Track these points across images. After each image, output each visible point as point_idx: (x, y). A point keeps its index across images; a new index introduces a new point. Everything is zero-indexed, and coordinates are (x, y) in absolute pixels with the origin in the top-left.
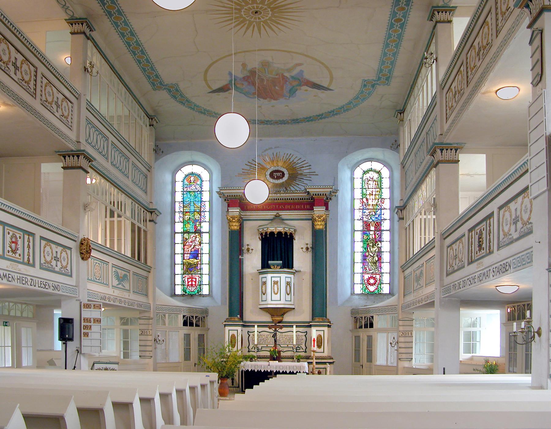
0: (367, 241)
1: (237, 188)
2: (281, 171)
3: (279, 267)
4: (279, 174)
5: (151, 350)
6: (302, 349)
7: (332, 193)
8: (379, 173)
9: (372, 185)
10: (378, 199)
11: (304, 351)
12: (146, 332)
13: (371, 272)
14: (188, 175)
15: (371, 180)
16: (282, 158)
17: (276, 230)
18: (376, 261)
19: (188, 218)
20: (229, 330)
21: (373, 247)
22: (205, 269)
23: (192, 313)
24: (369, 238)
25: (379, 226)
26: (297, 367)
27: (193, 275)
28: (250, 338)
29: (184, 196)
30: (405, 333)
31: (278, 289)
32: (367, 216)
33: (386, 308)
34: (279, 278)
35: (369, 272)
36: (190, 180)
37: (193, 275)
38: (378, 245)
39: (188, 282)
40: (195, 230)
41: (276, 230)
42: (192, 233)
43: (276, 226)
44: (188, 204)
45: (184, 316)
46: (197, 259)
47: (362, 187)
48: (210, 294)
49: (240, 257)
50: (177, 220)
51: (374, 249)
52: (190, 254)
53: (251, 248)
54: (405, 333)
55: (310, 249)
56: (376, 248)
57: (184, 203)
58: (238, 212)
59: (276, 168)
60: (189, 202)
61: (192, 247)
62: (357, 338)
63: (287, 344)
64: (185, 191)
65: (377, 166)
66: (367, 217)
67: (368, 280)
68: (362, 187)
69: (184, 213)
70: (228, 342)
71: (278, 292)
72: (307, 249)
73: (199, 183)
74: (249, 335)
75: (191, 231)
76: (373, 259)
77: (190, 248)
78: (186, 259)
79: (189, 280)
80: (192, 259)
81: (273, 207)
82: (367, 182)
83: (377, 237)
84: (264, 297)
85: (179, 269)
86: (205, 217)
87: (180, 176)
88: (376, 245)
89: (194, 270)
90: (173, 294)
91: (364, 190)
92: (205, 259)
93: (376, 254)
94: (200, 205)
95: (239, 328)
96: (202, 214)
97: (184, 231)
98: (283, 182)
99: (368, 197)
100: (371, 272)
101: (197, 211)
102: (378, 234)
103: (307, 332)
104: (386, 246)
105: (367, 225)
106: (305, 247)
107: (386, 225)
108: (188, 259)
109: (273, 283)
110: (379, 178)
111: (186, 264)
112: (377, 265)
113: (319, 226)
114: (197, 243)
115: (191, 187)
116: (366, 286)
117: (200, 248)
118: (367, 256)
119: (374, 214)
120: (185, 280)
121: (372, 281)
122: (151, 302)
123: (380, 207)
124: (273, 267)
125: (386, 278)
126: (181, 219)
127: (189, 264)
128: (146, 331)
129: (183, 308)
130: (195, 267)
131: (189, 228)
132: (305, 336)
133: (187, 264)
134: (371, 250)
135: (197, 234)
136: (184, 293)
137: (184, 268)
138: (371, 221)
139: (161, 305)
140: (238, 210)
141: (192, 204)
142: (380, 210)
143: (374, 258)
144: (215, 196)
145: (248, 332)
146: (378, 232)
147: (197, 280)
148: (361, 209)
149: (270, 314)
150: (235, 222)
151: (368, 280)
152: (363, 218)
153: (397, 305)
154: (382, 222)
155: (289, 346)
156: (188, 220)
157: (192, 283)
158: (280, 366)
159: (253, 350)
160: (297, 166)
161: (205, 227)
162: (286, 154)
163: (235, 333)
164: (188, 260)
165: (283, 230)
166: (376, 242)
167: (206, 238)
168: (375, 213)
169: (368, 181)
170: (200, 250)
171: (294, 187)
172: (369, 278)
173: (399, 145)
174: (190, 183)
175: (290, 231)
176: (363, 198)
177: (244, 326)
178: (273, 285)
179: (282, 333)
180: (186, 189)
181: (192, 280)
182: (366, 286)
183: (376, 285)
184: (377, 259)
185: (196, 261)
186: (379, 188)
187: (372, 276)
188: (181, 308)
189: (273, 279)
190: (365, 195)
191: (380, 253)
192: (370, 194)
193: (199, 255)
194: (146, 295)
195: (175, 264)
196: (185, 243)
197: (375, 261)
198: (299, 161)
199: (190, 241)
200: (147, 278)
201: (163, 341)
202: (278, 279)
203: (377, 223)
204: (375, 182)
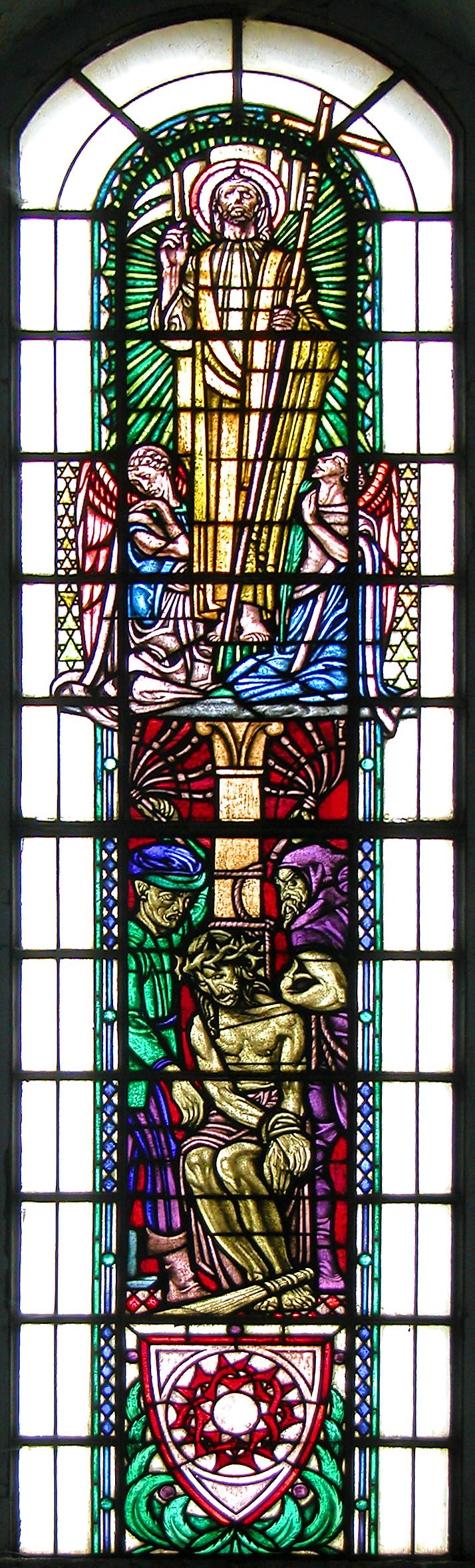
0: (172, 951)
10: (312, 460)
13: (224, 1303)
18: (297, 1181)
24: (197, 915)
25: (314, 759)
27: (310, 418)
32: (173, 657)
35: (199, 1307)
37: (310, 418)
38: (300, 986)
47: (120, 313)
51: (263, 1033)
56: (281, 1021)
66: (177, 671)
68: (120, 313)
76: (258, 1160)
88: (286, 982)
93: (291, 1103)
100: (224, 1303)
102: (300, 872)
112: (305, 1224)
116: (173, 1469)
118: (193, 1129)
119: (251, 627)
123: (339, 551)
134: (228, 1038)
142: (335, 592)
143: (273, 1153)
148: (103, 578)
152: (125, 679)
168: (270, 625)
182: (173, 1469)
183: (281, 1451)
186: (332, 334)
187: (232, 1358)
190: (151, 410)
197: (279, 1182)
203: (293, 725)
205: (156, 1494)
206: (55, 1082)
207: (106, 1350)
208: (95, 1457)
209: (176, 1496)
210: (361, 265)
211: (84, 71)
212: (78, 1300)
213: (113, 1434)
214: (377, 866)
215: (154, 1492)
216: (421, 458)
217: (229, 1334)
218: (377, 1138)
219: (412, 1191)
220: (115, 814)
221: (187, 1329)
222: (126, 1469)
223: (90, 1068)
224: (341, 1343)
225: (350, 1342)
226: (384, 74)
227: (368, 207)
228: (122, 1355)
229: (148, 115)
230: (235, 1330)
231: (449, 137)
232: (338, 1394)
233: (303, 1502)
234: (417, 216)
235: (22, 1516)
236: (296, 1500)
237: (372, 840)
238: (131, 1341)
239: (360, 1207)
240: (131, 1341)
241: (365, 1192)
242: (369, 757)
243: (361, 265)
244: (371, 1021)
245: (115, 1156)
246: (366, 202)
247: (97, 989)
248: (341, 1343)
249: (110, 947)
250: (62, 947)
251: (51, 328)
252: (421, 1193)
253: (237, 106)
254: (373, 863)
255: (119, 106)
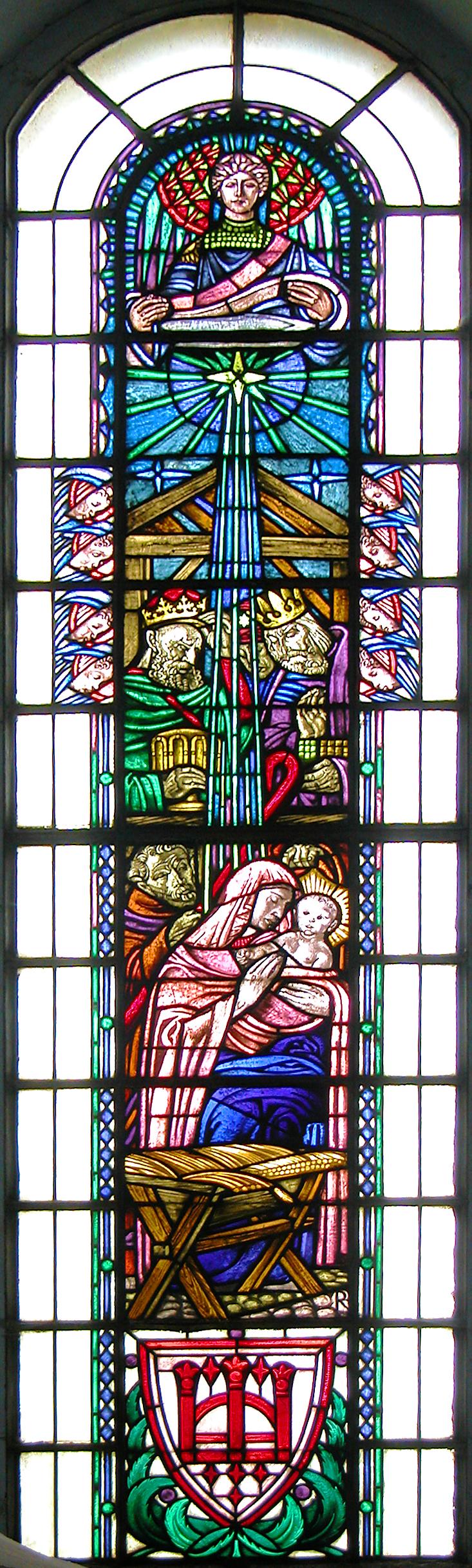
205: (157, 1498)
206: (53, 1454)
207: (105, 1431)
208: (96, 1294)
209: (176, 1499)
210: (365, 259)
211: (81, 68)
212: (77, 1307)
213: (113, 1439)
214: (377, 870)
215: (154, 1495)
216: (422, 459)
217: (230, 1338)
218: (378, 860)
219: (415, 1195)
220: (114, 1552)
221: (187, 1335)
222: (127, 1473)
223: (88, 1318)
224: (342, 1345)
225: (353, 1344)
226: (392, 66)
227: (372, 202)
228: (122, 1361)
229: (146, 113)
230: (235, 1333)
231: (456, 130)
232: (340, 1396)
233: (307, 1502)
234: (424, 210)
235: (20, 1277)
236: (297, 1500)
237: (372, 844)
238: (130, 1346)
239: (361, 1452)
240: (130, 1346)
241: (367, 1195)
242: (370, 762)
243: (365, 259)
244: (372, 773)
245: (112, 1183)
246: (371, 197)
247: (93, 746)
248: (342, 1345)
249: (106, 954)
250: (58, 955)
251: (49, 456)
252: (423, 952)
253: (238, 103)
254: (374, 866)
255: (118, 103)
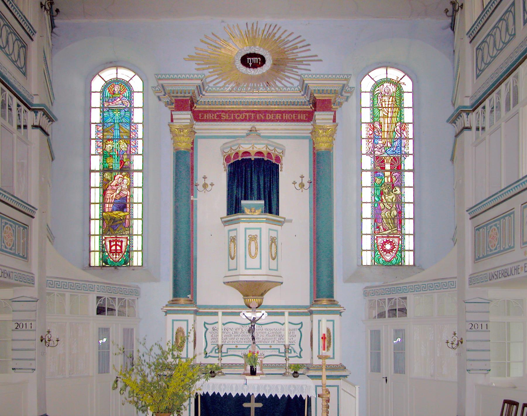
1: (187, 76)
2: (260, 55)
3: (258, 212)
4: (255, 60)
5: (33, 358)
6: (295, 352)
7: (343, 93)
8: (397, 84)
9: (387, 103)
11: (297, 356)
12: (24, 326)
14: (110, 83)
15: (386, 94)
16: (261, 33)
17: (253, 148)
19: (111, 148)
20: (173, 321)
21: (389, 194)
22: (137, 227)
23: (113, 294)
24: (383, 182)
26: (295, 388)
28: (209, 335)
29: (105, 114)
30: (476, 325)
31: (256, 248)
32: (380, 149)
33: (433, 282)
34: (259, 230)
35: (384, 233)
36: (114, 90)
38: (395, 191)
39: (111, 247)
40: (121, 168)
41: (253, 148)
42: (117, 171)
43: (254, 142)
44: (110, 128)
45: (98, 298)
46: (123, 212)
47: (373, 105)
48: (145, 265)
49: (192, 198)
50: (93, 151)
51: (391, 197)
52: (113, 203)
53: (208, 182)
54: (476, 325)
55: (307, 185)
56: (393, 195)
57: (103, 126)
58: (187, 119)
59: (252, 51)
60: (112, 124)
61: (118, 192)
62: (376, 335)
63: (270, 343)
64: (106, 108)
65: (394, 74)
67: (383, 245)
69: (105, 141)
70: (171, 342)
71: (256, 254)
72: (302, 185)
73: (126, 94)
74: (207, 329)
75: (116, 169)
77: (115, 194)
78: (107, 210)
79: (112, 244)
80: (117, 212)
81: (246, 116)
82: (380, 97)
83: (394, 181)
84: (233, 263)
85: (95, 227)
86: (136, 147)
87: (97, 84)
88: (393, 191)
89: (119, 228)
90: (88, 265)
91: (376, 111)
92: (137, 211)
94: (128, 128)
95: (190, 317)
96: (132, 143)
97: (103, 168)
98: (263, 73)
99: (382, 120)
100: (386, 232)
101: (125, 137)
102: (395, 176)
103: (302, 323)
104: (408, 195)
105: (379, 161)
106: (299, 181)
107: (408, 163)
108: (111, 212)
109: (248, 238)
110: (398, 92)
111: (107, 219)
112: (396, 222)
113: (323, 146)
114: (124, 187)
115: (115, 101)
116: (381, 254)
117: (129, 194)
118: (383, 210)
119: (389, 145)
120: (105, 243)
121: (388, 247)
122: (35, 270)
123: (399, 135)
124: (249, 210)
125: (409, 243)
126: (100, 151)
127: (113, 219)
128: (480, 324)
129: (96, 284)
130: (120, 224)
131: (111, 164)
132: (299, 329)
133: (109, 218)
135: (124, 173)
136: (104, 264)
137: (103, 224)
138: (386, 155)
139: (57, 278)
140: (189, 117)
141: (117, 127)
144: (153, 98)
145: (205, 323)
146: (396, 174)
147: (124, 244)
149: (242, 293)
150: (183, 136)
151: (383, 245)
153: (456, 278)
154: (403, 158)
155: (273, 347)
156: (111, 150)
157: (116, 248)
158: (266, 386)
159: (213, 354)
160: (286, 46)
161: (137, 162)
162: (268, 27)
163: (183, 325)
164: (110, 214)
165: (264, 149)
166: (393, 186)
167: (138, 179)
168: (391, 145)
169: (382, 97)
170: (128, 197)
171: (280, 82)
172: (385, 243)
173: (462, 5)
174: (114, 94)
175: (276, 152)
176: (374, 122)
177: (196, 313)
178: (248, 241)
179: (244, 324)
180: (107, 104)
181: (116, 243)
182: (381, 254)
184: (395, 213)
185: (122, 214)
188: (93, 284)
189: (249, 232)
191: (399, 203)
192: (384, 117)
193: (128, 205)
194: (23, 257)
195: (90, 219)
196: (106, 187)
198: (290, 38)
199: (114, 183)
200: (25, 227)
201: (58, 341)
202: (257, 232)
203: (394, 158)
204: (391, 98)
